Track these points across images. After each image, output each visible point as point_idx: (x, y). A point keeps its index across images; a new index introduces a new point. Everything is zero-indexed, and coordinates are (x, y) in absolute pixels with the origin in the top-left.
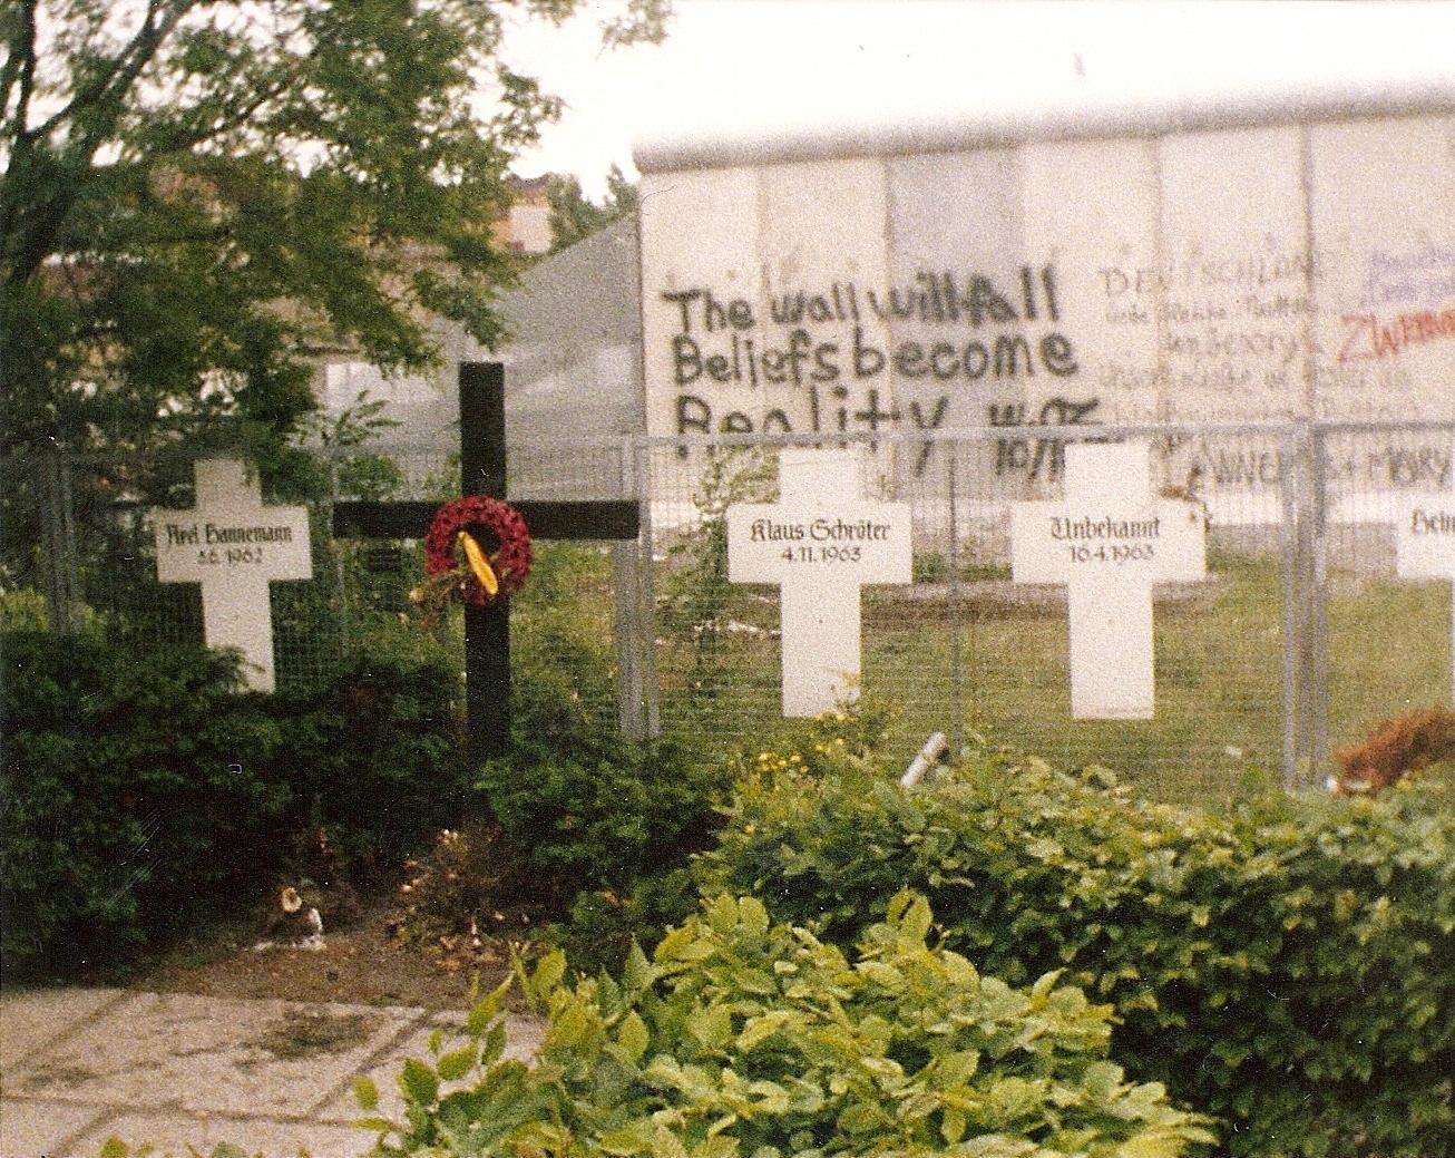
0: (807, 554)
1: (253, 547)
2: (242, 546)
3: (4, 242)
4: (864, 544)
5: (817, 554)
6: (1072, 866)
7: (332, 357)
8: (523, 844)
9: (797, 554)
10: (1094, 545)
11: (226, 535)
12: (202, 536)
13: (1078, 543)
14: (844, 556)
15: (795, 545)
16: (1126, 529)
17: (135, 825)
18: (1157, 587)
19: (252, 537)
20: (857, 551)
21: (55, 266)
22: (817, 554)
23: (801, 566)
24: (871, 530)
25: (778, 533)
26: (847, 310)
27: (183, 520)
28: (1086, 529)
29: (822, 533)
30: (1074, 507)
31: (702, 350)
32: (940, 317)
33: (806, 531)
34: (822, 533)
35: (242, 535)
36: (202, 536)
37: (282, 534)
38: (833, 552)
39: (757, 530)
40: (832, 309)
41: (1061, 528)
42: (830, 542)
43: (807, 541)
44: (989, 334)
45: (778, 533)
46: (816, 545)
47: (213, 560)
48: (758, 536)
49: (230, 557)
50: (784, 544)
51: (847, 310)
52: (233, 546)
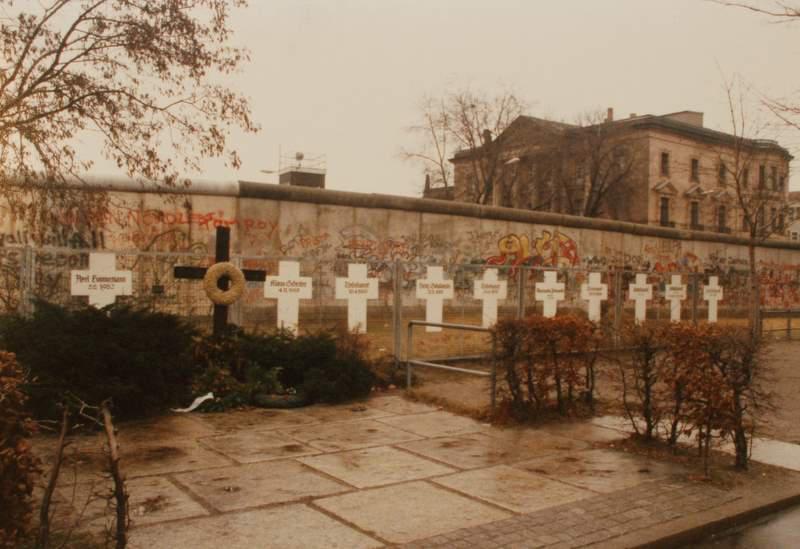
0: (285, 290)
1: (110, 283)
3: (797, 276)
6: (145, 305)
8: (517, 336)
11: (100, 279)
12: (90, 280)
16: (362, 285)
17: (536, 365)
18: (445, 300)
24: (116, 280)
25: (278, 284)
26: (22, 239)
27: (83, 273)
30: (674, 285)
32: (60, 245)
35: (107, 279)
36: (90, 280)
37: (123, 280)
40: (17, 239)
44: (77, 251)
45: (278, 284)
47: (95, 287)
49: (102, 287)
51: (22, 239)
52: (103, 283)
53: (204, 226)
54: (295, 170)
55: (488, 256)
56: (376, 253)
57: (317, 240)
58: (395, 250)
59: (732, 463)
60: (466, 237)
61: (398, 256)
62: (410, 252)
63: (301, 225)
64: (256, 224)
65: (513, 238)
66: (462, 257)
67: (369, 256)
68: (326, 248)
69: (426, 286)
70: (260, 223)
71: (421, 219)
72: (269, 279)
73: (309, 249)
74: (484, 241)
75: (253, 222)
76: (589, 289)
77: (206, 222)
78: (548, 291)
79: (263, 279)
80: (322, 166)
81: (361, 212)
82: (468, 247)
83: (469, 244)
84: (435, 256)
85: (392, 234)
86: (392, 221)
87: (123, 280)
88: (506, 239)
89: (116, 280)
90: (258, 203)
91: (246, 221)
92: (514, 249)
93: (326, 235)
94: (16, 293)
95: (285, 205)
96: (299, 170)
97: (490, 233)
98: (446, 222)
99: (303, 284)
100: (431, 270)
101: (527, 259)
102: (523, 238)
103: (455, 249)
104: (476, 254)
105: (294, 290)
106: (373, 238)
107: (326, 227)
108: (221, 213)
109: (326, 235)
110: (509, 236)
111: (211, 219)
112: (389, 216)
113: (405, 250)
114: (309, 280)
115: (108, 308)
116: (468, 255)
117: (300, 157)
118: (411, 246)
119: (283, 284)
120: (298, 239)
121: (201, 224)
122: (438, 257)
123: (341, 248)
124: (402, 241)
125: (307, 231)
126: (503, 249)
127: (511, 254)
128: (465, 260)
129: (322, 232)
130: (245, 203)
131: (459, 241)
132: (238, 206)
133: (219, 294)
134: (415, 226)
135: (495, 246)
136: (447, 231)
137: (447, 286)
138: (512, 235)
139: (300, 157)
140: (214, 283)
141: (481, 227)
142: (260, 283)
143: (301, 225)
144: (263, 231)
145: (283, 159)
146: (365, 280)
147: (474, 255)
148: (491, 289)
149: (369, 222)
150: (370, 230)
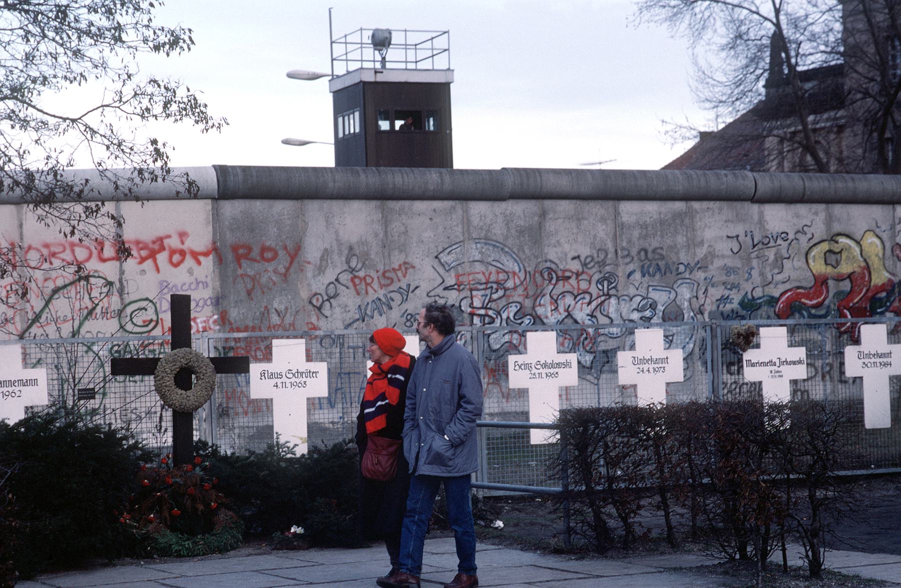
1: (16, 389)
2: (10, 389)
4: (308, 380)
5: (288, 385)
7: (763, 218)
9: (280, 385)
10: (646, 367)
13: (866, 361)
14: (300, 385)
15: (279, 381)
16: (657, 361)
19: (16, 384)
20: (557, 373)
21: (766, 92)
22: (288, 385)
23: (281, 390)
24: (25, 383)
25: (272, 376)
27: (520, 359)
28: (869, 355)
29: (290, 376)
30: (639, 352)
31: (588, 254)
33: (284, 374)
34: (539, 367)
35: (11, 383)
37: (34, 382)
38: (295, 384)
39: (263, 374)
41: (637, 361)
42: (293, 380)
43: (284, 379)
45: (272, 376)
46: (288, 381)
48: (263, 378)
50: (274, 381)
53: (149, 262)
54: (369, 77)
55: (782, 288)
56: (518, 296)
57: (387, 278)
58: (560, 287)
59: (808, 573)
60: (724, 247)
61: (569, 300)
62: (594, 290)
63: (351, 248)
64: (255, 253)
65: (843, 240)
66: (716, 293)
67: (503, 302)
68: (406, 293)
69: (527, 366)
70: (264, 249)
71: (617, 214)
72: (255, 369)
73: (372, 296)
74: (771, 254)
75: (250, 249)
76: (861, 355)
77: (153, 255)
78: (771, 363)
79: (246, 370)
80: (441, 63)
81: (478, 209)
82: (728, 271)
83: (737, 263)
84: (654, 295)
85: (552, 254)
86: (550, 226)
87: (34, 382)
88: (825, 246)
89: (25, 383)
90: (258, 206)
91: (235, 249)
92: (845, 268)
93: (407, 266)
94: (381, 293)
95: (313, 207)
96: (380, 78)
97: (784, 235)
98: (678, 216)
99: (313, 374)
100: (534, 338)
101: (882, 288)
102: (871, 241)
103: (700, 275)
104: (752, 287)
105: (298, 385)
106: (514, 267)
107: (403, 249)
108: (183, 235)
109: (407, 266)
110: (833, 239)
111: (162, 248)
112: (543, 215)
113: (584, 285)
114: (322, 368)
115: (20, 423)
116: (734, 286)
117: (381, 41)
118: (596, 277)
119: (280, 375)
120: (345, 278)
121: (143, 260)
122: (661, 297)
123: (439, 291)
124: (575, 266)
125: (365, 259)
126: (819, 267)
127: (839, 279)
128: (723, 300)
129: (397, 259)
130: (231, 209)
131: (711, 255)
132: (216, 216)
133: (178, 396)
134: (603, 232)
135: (799, 263)
136: (681, 240)
137: (567, 365)
138: (840, 234)
139: (381, 41)
140: (170, 381)
141: (761, 221)
142: (241, 378)
143: (351, 248)
144: (270, 267)
145: (339, 50)
146: (305, 366)
147: (748, 287)
148: (651, 366)
149: (498, 231)
150: (501, 247)
